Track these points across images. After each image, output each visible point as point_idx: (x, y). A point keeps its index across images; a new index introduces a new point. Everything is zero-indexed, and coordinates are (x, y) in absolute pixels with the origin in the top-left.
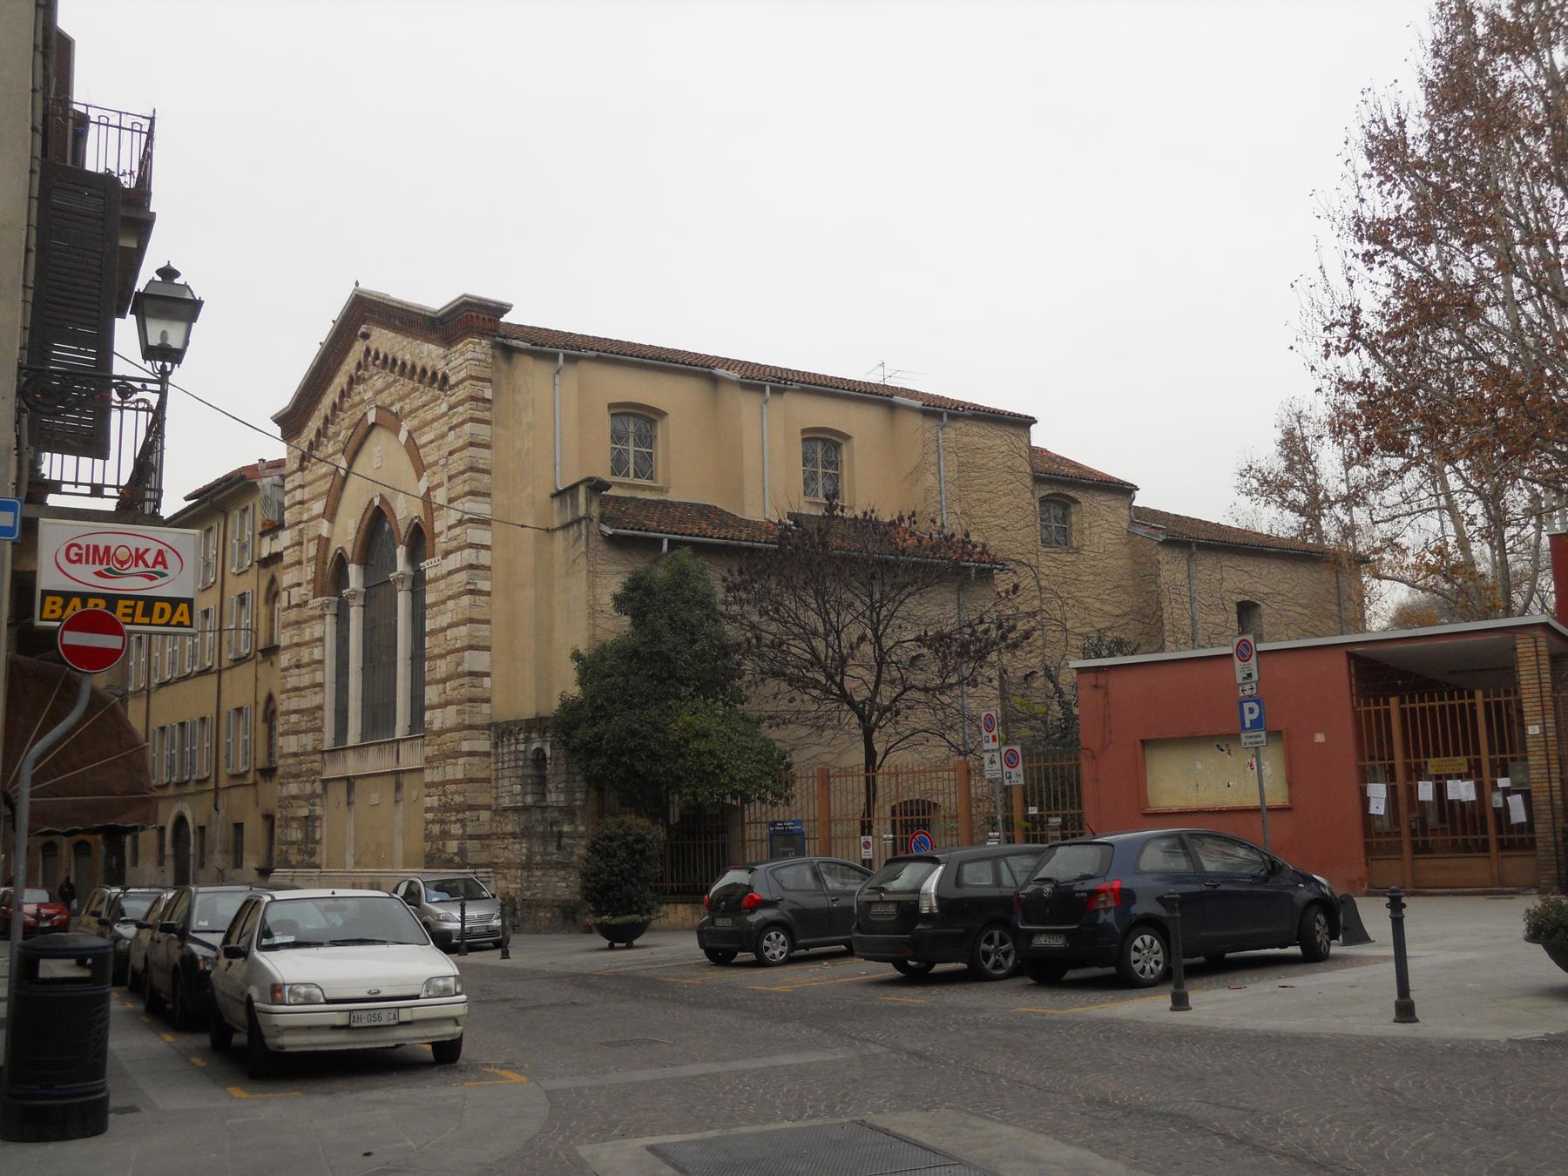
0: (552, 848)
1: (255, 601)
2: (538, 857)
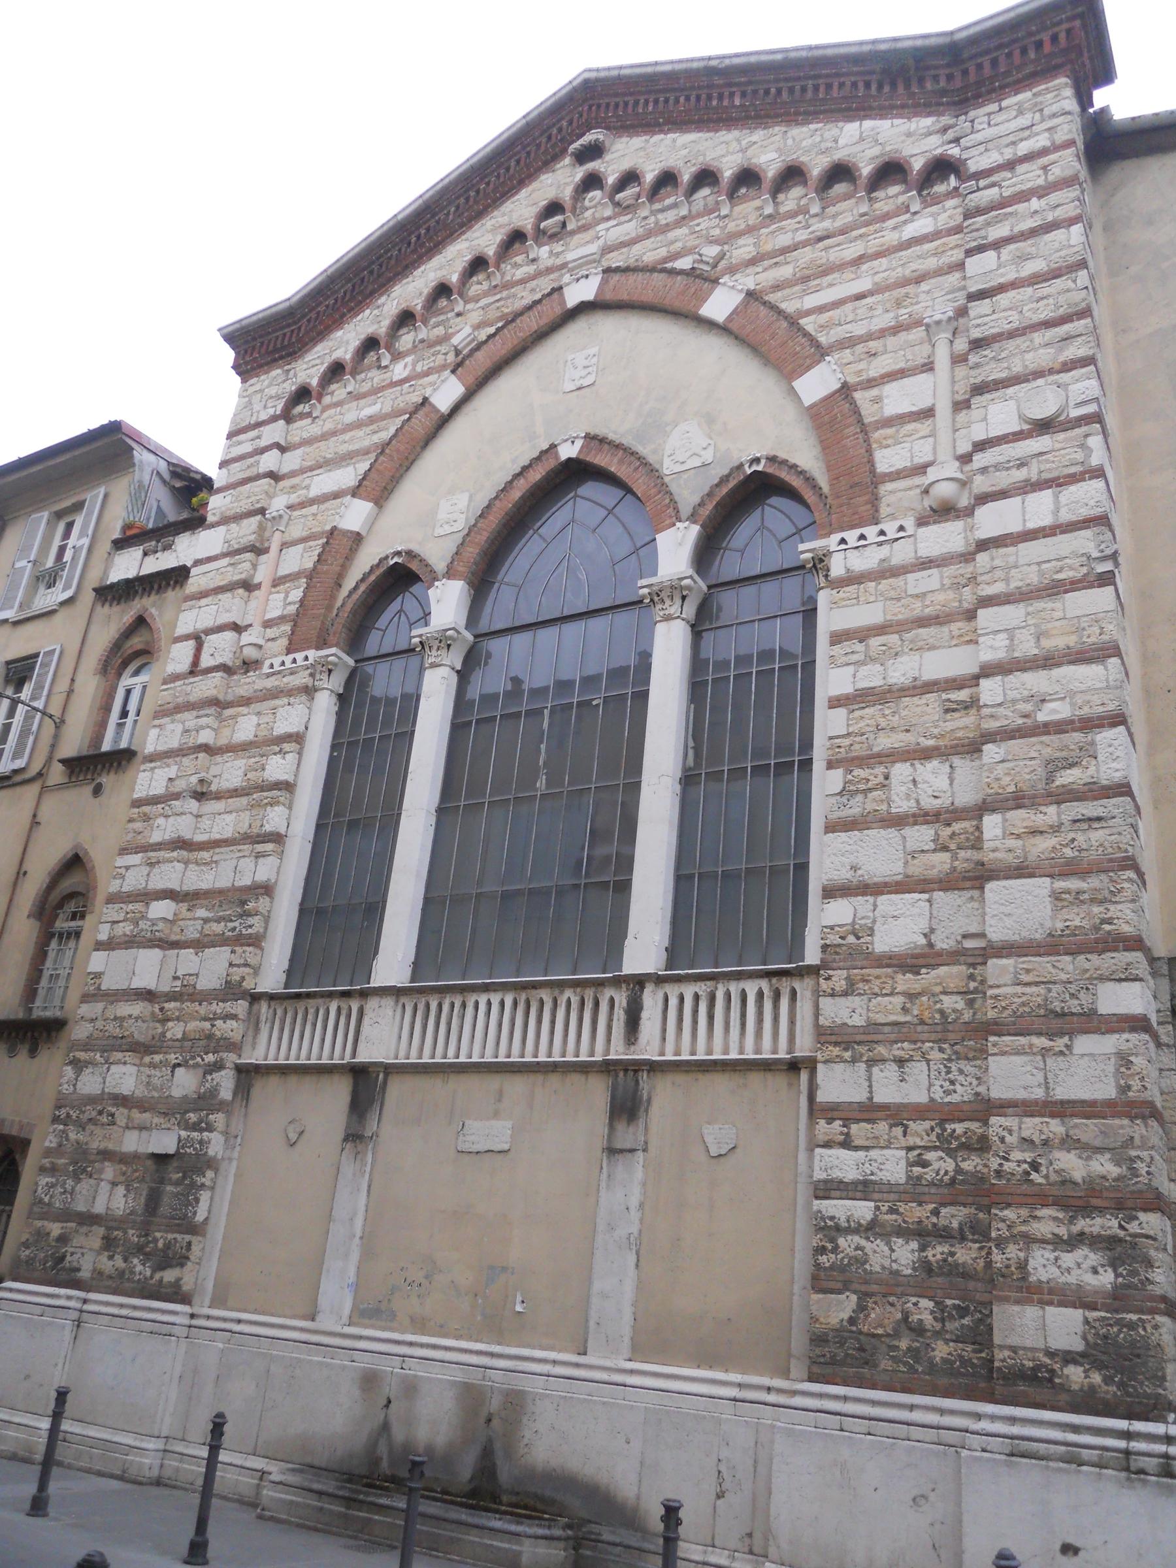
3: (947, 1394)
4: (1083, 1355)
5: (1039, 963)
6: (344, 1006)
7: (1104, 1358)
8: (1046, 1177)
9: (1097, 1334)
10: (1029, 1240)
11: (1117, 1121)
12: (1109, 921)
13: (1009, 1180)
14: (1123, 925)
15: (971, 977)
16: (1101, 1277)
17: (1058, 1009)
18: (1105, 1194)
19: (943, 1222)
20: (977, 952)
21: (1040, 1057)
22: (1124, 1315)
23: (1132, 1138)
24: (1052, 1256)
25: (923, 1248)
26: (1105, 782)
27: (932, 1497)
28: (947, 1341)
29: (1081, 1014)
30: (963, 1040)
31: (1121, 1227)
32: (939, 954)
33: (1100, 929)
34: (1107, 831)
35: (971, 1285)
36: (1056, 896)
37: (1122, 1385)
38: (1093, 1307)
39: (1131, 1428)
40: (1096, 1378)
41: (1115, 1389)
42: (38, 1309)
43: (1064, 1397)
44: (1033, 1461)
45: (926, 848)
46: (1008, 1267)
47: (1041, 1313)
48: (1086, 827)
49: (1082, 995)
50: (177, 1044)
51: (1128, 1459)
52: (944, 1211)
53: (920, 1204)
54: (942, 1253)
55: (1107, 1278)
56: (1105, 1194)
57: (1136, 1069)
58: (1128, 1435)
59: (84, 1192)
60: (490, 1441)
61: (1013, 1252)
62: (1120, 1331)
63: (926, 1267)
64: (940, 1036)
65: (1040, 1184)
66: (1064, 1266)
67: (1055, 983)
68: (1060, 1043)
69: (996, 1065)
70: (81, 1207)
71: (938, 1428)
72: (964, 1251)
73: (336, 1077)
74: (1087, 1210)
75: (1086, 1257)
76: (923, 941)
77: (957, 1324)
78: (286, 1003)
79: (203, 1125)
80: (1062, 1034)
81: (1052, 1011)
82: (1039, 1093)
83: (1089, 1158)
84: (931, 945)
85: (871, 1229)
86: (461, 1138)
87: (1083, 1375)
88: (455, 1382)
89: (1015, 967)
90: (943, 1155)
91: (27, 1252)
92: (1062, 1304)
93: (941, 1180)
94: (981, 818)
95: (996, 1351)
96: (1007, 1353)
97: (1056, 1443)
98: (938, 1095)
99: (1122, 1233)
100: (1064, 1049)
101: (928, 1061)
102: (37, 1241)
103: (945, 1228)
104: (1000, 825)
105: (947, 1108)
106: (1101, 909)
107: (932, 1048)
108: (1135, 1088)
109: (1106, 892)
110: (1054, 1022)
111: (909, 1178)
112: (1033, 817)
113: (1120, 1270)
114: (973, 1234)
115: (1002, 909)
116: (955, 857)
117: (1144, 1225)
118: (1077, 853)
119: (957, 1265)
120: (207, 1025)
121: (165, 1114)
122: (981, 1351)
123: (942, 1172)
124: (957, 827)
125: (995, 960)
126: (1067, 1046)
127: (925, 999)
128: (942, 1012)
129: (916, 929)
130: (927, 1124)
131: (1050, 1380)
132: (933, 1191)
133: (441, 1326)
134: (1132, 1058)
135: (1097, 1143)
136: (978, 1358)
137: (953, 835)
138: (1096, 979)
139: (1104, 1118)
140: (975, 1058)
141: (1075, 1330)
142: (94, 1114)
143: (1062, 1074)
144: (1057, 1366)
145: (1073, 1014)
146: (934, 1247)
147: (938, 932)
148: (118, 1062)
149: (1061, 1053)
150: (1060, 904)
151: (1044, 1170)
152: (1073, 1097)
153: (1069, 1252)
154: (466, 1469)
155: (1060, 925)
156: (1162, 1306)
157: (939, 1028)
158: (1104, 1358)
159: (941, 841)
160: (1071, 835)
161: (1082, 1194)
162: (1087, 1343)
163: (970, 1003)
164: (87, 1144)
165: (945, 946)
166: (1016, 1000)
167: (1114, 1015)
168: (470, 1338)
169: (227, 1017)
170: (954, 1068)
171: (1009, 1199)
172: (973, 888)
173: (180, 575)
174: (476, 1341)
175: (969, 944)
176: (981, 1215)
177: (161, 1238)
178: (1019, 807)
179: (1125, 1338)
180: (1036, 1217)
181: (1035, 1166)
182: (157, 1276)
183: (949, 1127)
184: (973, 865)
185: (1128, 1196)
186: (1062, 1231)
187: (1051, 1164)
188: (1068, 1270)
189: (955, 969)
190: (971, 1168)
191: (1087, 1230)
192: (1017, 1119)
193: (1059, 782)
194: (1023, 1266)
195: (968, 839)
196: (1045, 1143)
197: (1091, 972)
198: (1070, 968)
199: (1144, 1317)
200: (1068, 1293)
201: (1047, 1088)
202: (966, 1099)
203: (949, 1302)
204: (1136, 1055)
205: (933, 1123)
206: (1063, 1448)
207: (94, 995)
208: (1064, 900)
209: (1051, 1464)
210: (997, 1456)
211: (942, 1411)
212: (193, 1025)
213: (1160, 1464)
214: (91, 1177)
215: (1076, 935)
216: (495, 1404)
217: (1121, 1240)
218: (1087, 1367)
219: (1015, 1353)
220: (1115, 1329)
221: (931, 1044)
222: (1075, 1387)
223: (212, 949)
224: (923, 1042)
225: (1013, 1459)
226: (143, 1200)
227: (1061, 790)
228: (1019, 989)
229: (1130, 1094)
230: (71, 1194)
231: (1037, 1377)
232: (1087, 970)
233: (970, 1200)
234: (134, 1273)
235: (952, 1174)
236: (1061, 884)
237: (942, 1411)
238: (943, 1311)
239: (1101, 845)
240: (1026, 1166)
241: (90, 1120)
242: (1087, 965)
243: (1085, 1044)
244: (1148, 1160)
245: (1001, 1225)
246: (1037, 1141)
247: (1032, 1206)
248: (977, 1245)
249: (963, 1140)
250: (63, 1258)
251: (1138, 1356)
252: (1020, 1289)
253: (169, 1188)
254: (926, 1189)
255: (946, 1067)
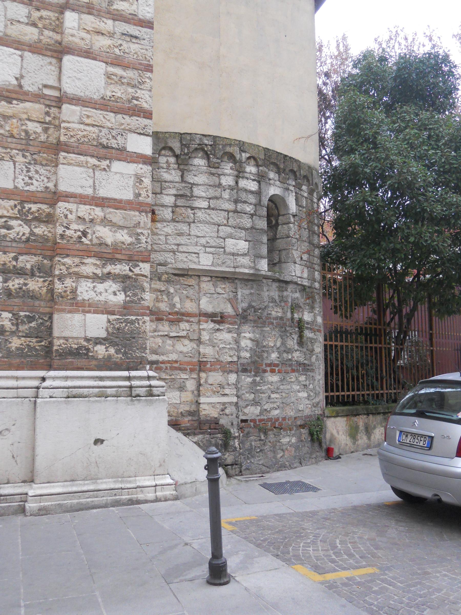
0: (292, 343)
1: (443, 328)
2: (274, 356)
3: (19, 368)
4: (105, 339)
5: (96, 113)
7: (116, 340)
8: (91, 240)
9: (114, 328)
10: (79, 276)
11: (132, 213)
12: (137, 99)
13: (68, 241)
14: (144, 103)
15: (47, 114)
16: (117, 297)
17: (105, 143)
18: (123, 252)
19: (20, 265)
20: (52, 99)
21: (91, 170)
22: (128, 317)
23: (139, 222)
24: (92, 286)
25: (5, 281)
26: (141, 17)
27: (13, 428)
28: (19, 337)
29: (117, 149)
30: (40, 152)
31: (130, 270)
32: (26, 93)
33: (131, 102)
34: (140, 46)
35: (37, 303)
36: (109, 76)
37: (125, 353)
38: (113, 313)
39: (131, 375)
40: (112, 351)
41: (121, 356)
43: (94, 363)
44: (81, 399)
45: (21, 20)
46: (65, 292)
47: (83, 318)
48: (129, 40)
49: (119, 138)
51: (131, 391)
52: (21, 258)
53: (5, 253)
54: (19, 284)
55: (121, 297)
56: (123, 252)
57: (144, 185)
58: (129, 378)
61: (69, 282)
62: (126, 325)
64: (24, 147)
65: (87, 245)
66: (98, 291)
67: (103, 127)
68: (105, 163)
69: (63, 170)
71: (17, 388)
72: (33, 283)
74: (113, 260)
75: (111, 286)
76: (15, 82)
77: (26, 327)
80: (105, 158)
81: (101, 144)
82: (90, 192)
83: (115, 232)
84: (20, 86)
87: (105, 350)
89: (81, 113)
90: (22, 223)
92: (95, 312)
93: (20, 239)
94: (62, 13)
95: (55, 341)
96: (62, 341)
97: (93, 387)
98: (20, 185)
99: (131, 274)
100: (106, 168)
101: (14, 163)
103: (22, 268)
104: (77, 21)
105: (26, 194)
106: (133, 90)
107: (18, 154)
108: (143, 196)
109: (137, 81)
110: (101, 150)
112: (98, 23)
113: (128, 293)
114: (40, 273)
115: (75, 74)
116: (41, 33)
117: (142, 269)
118: (122, 54)
119: (28, 291)
122: (41, 342)
123: (21, 234)
124: (44, 13)
125: (68, 105)
126: (108, 166)
127: (15, 121)
128: (26, 132)
129: (10, 72)
130: (12, 203)
131: (87, 354)
132: (14, 245)
134: (143, 179)
135: (121, 223)
136: (39, 346)
137: (41, 18)
138: (127, 130)
139: (125, 210)
140: (46, 165)
141: (102, 326)
143: (104, 182)
144: (90, 347)
145: (113, 148)
146: (13, 280)
147: (26, 79)
149: (104, 169)
150: (110, 81)
151: (89, 236)
152: (109, 196)
153: (101, 283)
154: (198, 312)
155: (109, 94)
156: (148, 312)
157: (24, 142)
158: (116, 340)
159: (32, 19)
160: (120, 42)
161: (111, 251)
162: (108, 333)
163: (46, 130)
165: (30, 89)
166: (80, 133)
167: (135, 153)
170: (32, 169)
171: (68, 252)
172: (52, 57)
175: (47, 92)
176: (45, 261)
178: (89, 13)
179: (128, 329)
180: (84, 263)
181: (85, 234)
183: (27, 206)
184: (53, 42)
185: (135, 254)
186: (99, 272)
187: (94, 233)
188: (101, 293)
189: (37, 106)
190: (40, 233)
191: (112, 271)
192: (75, 205)
193: (115, 7)
194: (74, 291)
195: (51, 24)
196: (92, 221)
197: (126, 125)
198: (113, 120)
199: (139, 318)
200: (100, 306)
201: (95, 189)
202: (39, 189)
203: (22, 314)
204: (145, 177)
205: (16, 202)
206: (97, 390)
208: (113, 79)
209: (91, 399)
210: (59, 399)
211: (17, 378)
213: (146, 391)
215: (117, 102)
217: (129, 277)
218: (107, 345)
219: (67, 341)
220: (124, 325)
221: (17, 151)
222: (100, 357)
224: (11, 149)
225: (69, 399)
227: (116, 12)
228: (82, 127)
229: (140, 198)
231: (79, 353)
232: (123, 124)
233: (39, 252)
235: (28, 235)
236: (111, 69)
237: (17, 378)
238: (17, 319)
239: (136, 53)
240: (79, 233)
242: (123, 121)
243: (117, 166)
244: (147, 235)
245: (62, 267)
246: (87, 220)
247: (82, 257)
248: (42, 279)
249: (37, 215)
251: (134, 338)
252: (72, 305)
254: (9, 244)
255: (26, 167)
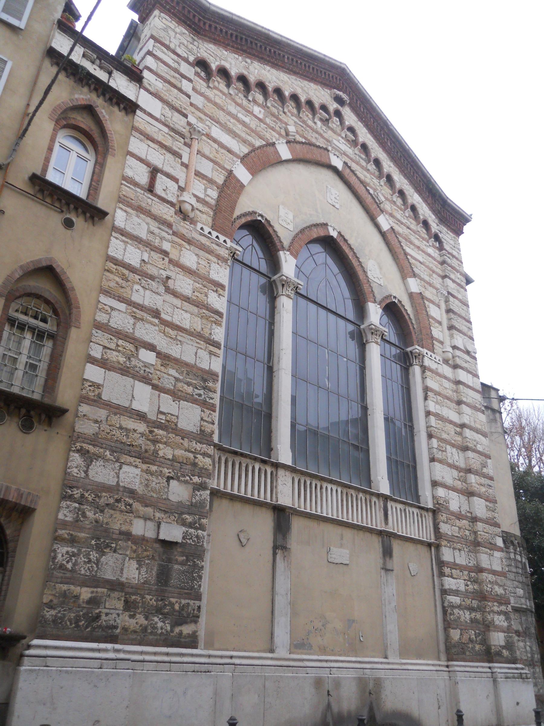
6: (262, 468)
42: (97, 663)
50: (169, 463)
59: (111, 563)
60: (371, 703)
63: (472, 620)
70: (109, 576)
73: (264, 510)
78: (227, 455)
79: (197, 525)
85: (459, 607)
86: (329, 555)
88: (353, 677)
91: (53, 612)
102: (63, 603)
111: (466, 590)
120: (191, 456)
121: (165, 512)
133: (332, 650)
142: (111, 501)
148: (130, 464)
164: (107, 524)
168: (345, 655)
169: (205, 455)
173: (130, 107)
174: (348, 656)
177: (177, 603)
182: (177, 630)
183: (471, 574)
207: (95, 401)
212: (179, 453)
214: (115, 551)
216: (371, 685)
223: (185, 402)
226: (154, 573)
230: (97, 565)
234: (156, 628)
241: (107, 505)
250: (98, 617)
253: (176, 567)
